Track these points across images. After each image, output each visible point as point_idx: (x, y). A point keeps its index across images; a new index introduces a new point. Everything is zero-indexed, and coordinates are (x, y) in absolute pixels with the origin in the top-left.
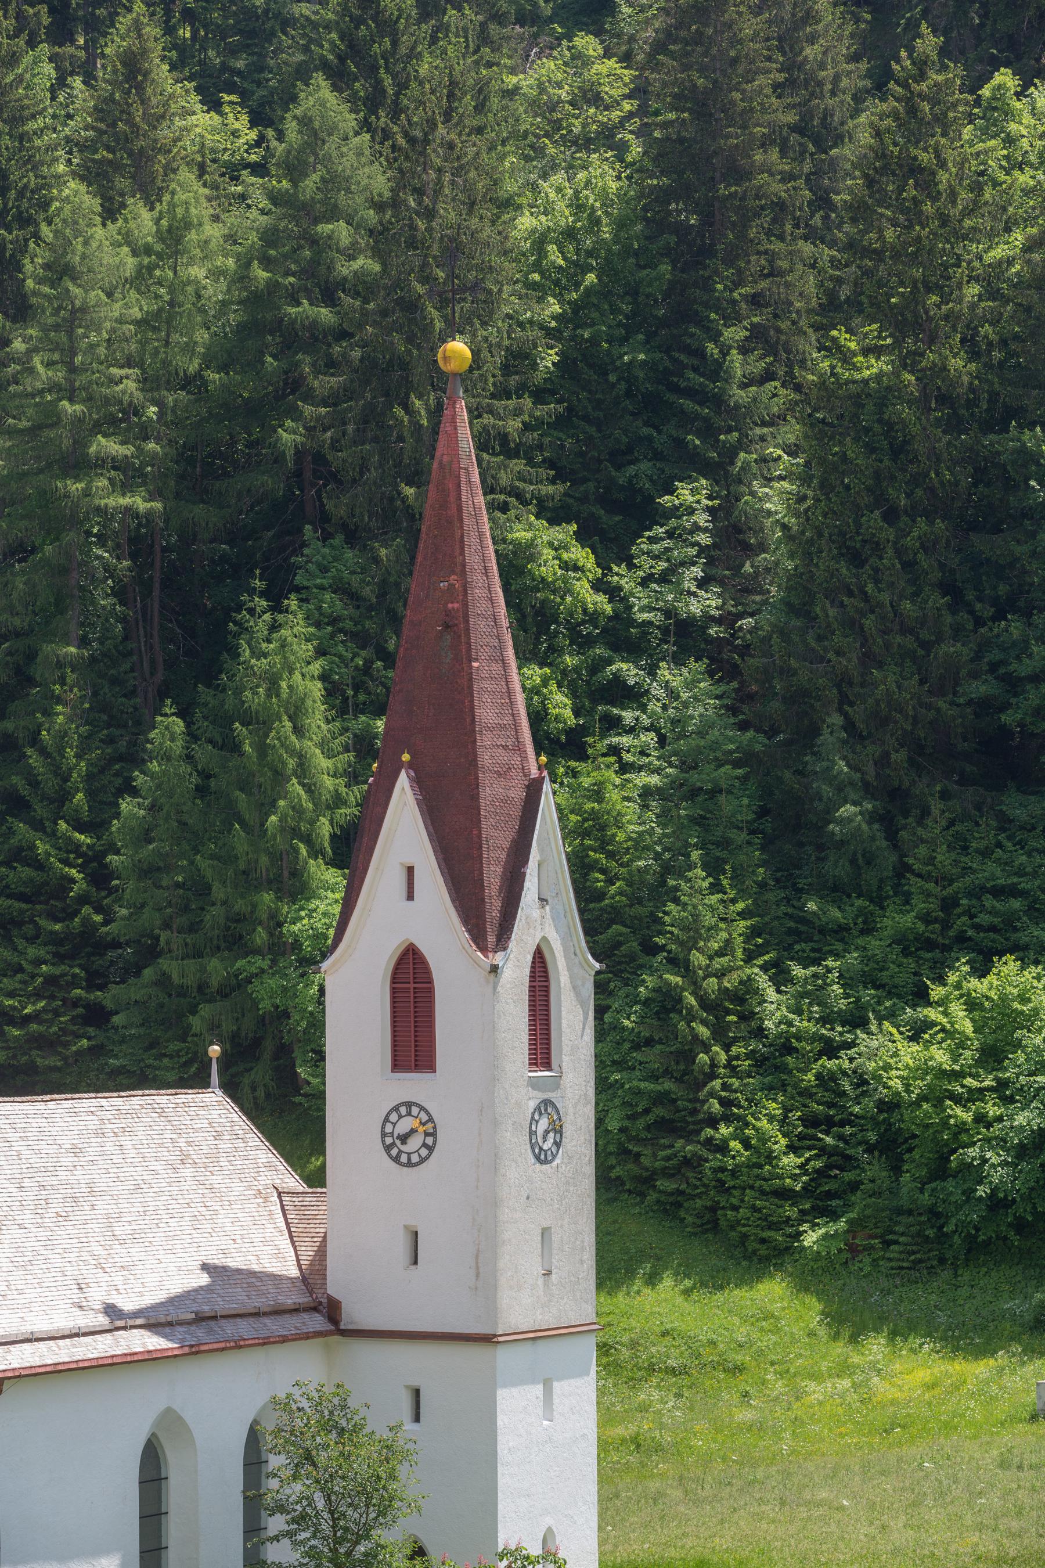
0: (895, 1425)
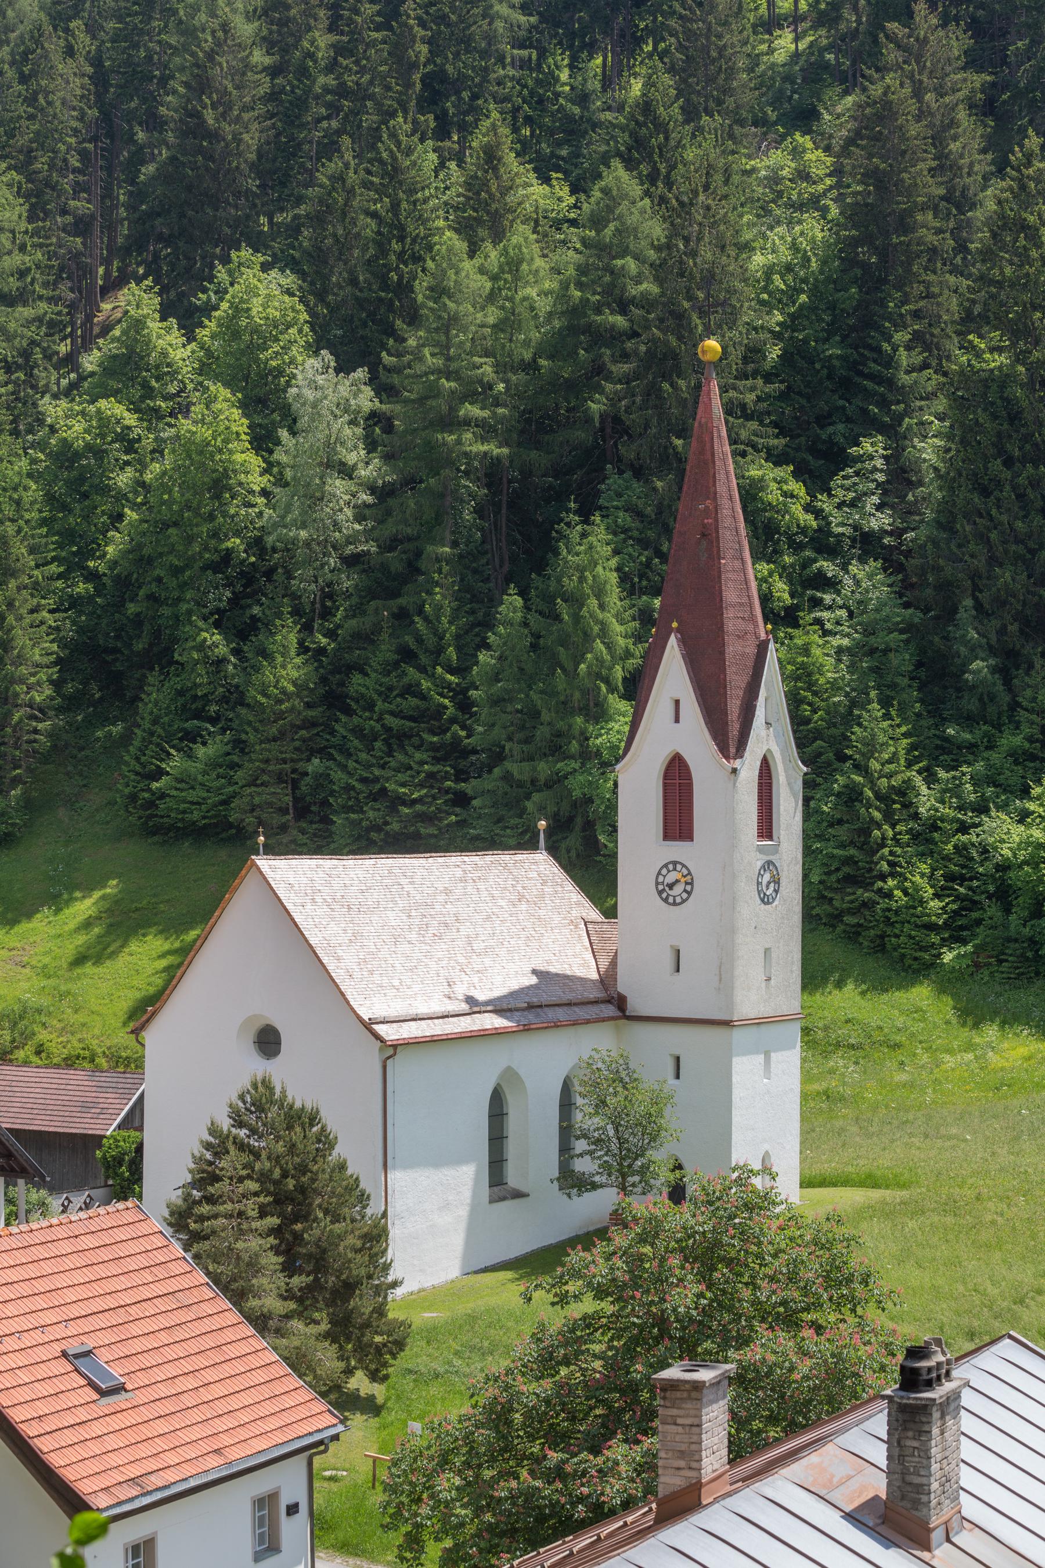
0: (1002, 1085)
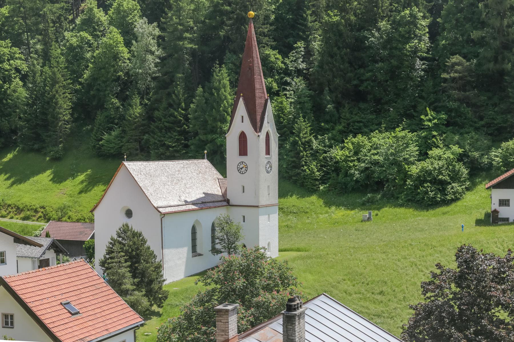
0: (336, 223)
